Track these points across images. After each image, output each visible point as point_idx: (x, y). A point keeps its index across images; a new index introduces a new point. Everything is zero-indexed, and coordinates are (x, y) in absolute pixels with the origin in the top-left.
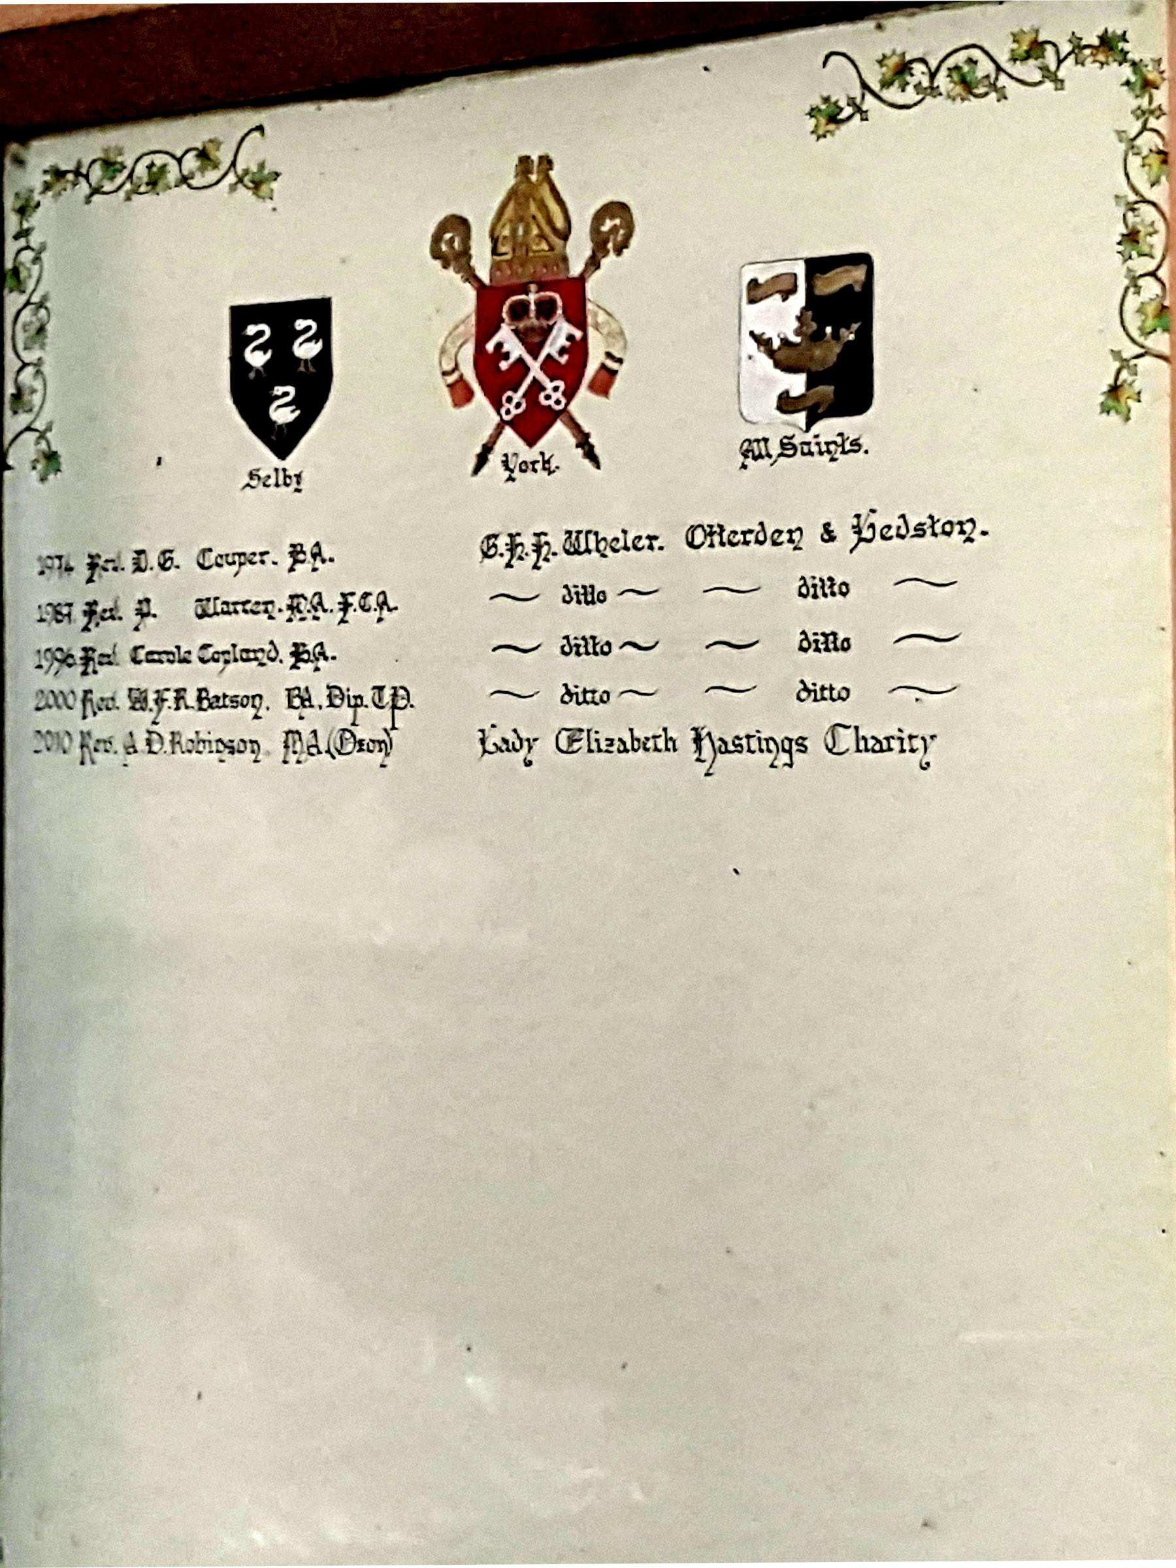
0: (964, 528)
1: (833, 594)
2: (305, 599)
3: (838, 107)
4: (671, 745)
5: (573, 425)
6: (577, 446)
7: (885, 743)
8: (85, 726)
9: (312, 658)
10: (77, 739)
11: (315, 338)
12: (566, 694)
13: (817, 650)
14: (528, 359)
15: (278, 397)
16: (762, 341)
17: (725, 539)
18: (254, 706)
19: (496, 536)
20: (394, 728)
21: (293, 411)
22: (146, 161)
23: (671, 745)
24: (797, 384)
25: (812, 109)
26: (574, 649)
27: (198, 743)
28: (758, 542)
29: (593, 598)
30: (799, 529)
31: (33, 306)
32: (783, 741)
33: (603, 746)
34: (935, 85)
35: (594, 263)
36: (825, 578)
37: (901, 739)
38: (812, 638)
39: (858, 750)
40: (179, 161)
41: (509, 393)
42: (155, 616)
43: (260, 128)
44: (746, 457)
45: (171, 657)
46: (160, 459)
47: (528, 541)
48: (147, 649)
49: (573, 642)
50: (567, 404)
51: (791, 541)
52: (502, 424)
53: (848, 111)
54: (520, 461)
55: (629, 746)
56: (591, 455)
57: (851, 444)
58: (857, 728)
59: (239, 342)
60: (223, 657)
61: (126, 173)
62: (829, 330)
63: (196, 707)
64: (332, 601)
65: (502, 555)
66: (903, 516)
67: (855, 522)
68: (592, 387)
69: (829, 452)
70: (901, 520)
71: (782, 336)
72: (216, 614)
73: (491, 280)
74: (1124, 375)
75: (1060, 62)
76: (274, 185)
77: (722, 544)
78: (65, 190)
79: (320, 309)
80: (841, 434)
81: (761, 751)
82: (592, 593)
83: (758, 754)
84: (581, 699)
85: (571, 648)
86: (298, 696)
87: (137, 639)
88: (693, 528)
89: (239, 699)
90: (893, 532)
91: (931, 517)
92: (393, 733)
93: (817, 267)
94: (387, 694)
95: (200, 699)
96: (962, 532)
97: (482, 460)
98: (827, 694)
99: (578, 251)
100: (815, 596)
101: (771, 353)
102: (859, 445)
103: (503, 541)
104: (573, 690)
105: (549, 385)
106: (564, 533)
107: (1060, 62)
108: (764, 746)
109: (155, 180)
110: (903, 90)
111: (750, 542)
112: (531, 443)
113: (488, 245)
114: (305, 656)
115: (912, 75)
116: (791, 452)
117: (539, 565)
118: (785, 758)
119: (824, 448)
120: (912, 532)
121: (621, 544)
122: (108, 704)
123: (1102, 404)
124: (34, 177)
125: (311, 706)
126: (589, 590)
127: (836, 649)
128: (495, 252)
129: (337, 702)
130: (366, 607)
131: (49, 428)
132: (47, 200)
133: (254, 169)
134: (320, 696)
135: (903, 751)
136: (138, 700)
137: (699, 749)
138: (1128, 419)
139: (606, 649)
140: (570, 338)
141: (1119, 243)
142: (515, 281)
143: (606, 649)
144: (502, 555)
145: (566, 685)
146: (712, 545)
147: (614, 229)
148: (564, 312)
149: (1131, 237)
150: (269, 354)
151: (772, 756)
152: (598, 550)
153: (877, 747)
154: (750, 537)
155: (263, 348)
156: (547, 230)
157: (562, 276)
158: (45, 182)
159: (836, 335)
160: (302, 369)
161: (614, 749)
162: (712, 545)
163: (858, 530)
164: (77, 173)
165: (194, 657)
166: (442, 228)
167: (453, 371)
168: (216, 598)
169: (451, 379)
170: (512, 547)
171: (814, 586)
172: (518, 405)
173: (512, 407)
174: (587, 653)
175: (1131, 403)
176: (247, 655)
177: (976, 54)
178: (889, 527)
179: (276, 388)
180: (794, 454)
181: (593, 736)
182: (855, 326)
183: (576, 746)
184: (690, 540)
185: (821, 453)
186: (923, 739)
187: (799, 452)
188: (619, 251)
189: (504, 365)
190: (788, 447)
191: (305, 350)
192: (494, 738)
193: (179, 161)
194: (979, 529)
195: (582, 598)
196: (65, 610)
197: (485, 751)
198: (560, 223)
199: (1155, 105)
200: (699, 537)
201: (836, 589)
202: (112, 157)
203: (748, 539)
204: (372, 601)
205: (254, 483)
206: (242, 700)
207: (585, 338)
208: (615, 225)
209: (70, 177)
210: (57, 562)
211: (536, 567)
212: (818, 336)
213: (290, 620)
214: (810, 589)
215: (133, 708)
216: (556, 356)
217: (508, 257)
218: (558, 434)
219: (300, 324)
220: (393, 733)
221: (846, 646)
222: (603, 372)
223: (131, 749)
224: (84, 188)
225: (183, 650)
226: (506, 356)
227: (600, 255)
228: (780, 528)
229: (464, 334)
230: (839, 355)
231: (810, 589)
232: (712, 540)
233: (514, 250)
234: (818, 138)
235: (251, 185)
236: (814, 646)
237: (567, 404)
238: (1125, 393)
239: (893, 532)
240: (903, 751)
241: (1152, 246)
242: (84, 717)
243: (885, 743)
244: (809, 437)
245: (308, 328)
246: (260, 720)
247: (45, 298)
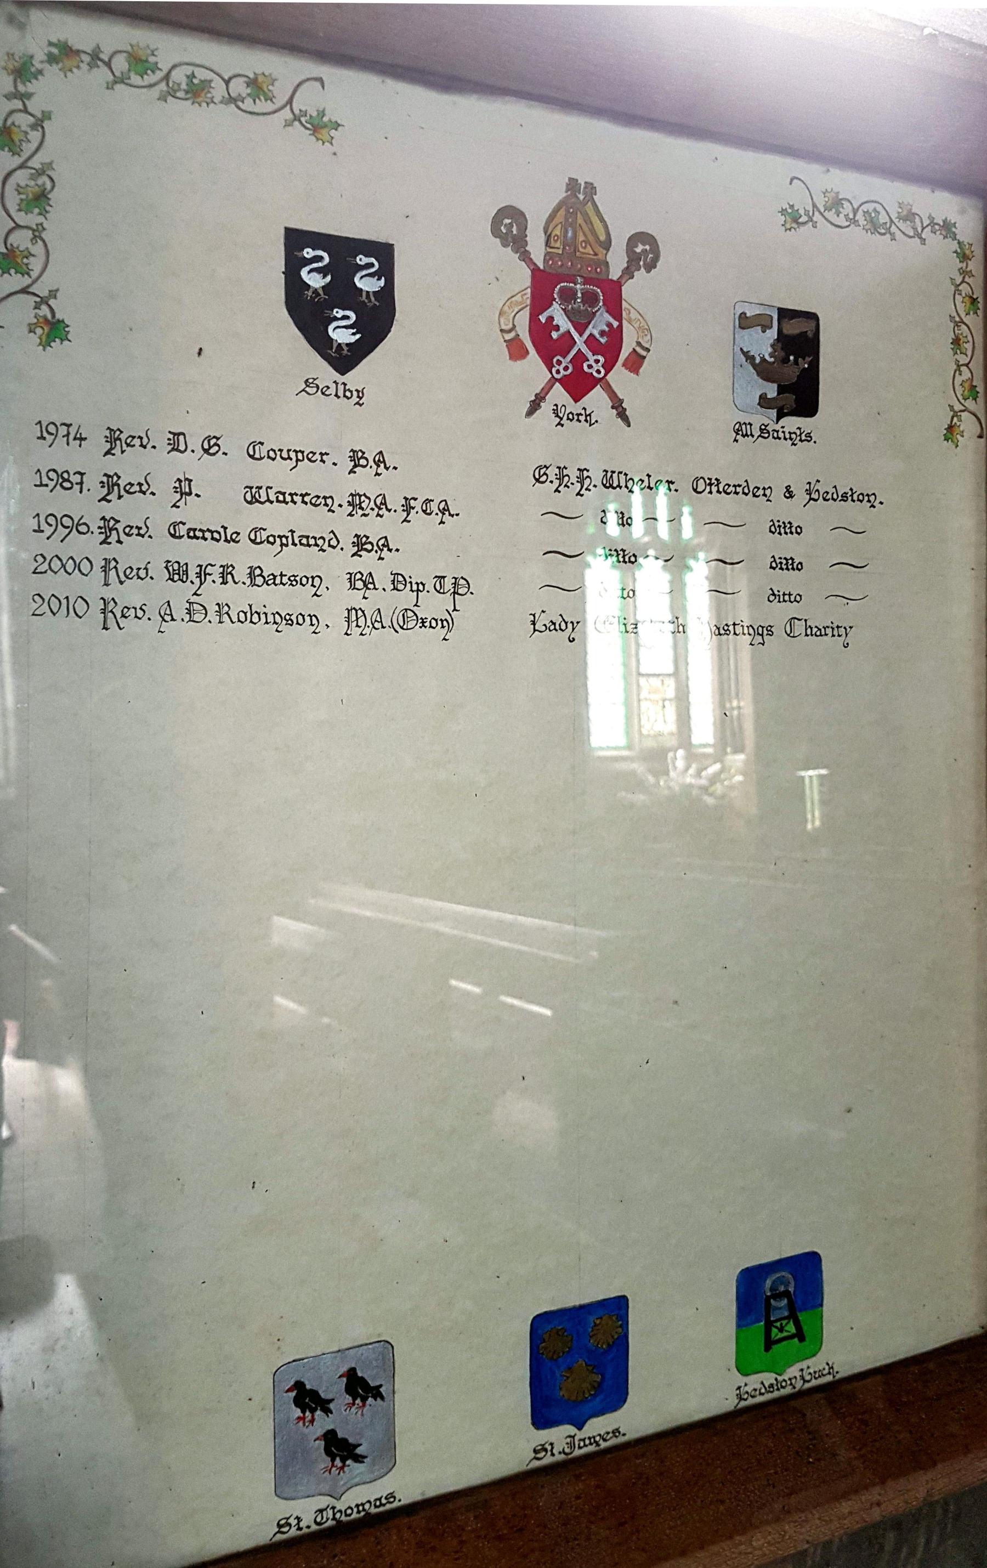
0: (868, 499)
3: (798, 213)
7: (823, 630)
8: (108, 593)
13: (781, 569)
14: (576, 335)
15: (336, 319)
18: (313, 585)
20: (455, 610)
21: (354, 334)
27: (251, 615)
28: (744, 493)
34: (856, 219)
36: (786, 522)
38: (778, 561)
39: (807, 635)
44: (738, 434)
46: (201, 349)
47: (573, 474)
50: (606, 375)
51: (765, 495)
57: (806, 436)
58: (806, 620)
60: (283, 541)
61: (159, 75)
62: (792, 358)
64: (395, 502)
65: (551, 482)
66: (835, 487)
67: (808, 487)
69: (791, 439)
70: (834, 489)
74: (955, 419)
75: (923, 229)
80: (799, 428)
87: (176, 515)
88: (697, 479)
90: (829, 496)
91: (851, 489)
92: (454, 614)
93: (784, 314)
95: (251, 575)
98: (787, 598)
100: (780, 533)
101: (755, 366)
103: (552, 472)
106: (602, 471)
107: (923, 229)
108: (746, 631)
110: (838, 216)
111: (739, 493)
112: (576, 401)
113: (542, 238)
114: (369, 547)
115: (843, 208)
117: (581, 493)
118: (759, 639)
119: (787, 436)
120: (840, 498)
122: (141, 573)
123: (944, 435)
128: (547, 244)
129: (401, 587)
130: (428, 511)
135: (833, 636)
136: (177, 573)
138: (957, 446)
139: (633, 559)
140: (609, 325)
141: (952, 343)
143: (633, 559)
144: (551, 482)
146: (711, 492)
147: (644, 251)
149: (956, 342)
150: (329, 278)
152: (626, 487)
153: (818, 633)
154: (739, 489)
155: (323, 271)
156: (591, 238)
159: (796, 362)
163: (809, 492)
165: (243, 537)
167: (510, 331)
169: (509, 336)
170: (561, 478)
171: (779, 526)
172: (566, 368)
175: (958, 436)
176: (306, 541)
177: (879, 208)
182: (808, 359)
184: (695, 487)
186: (845, 628)
187: (771, 436)
192: (541, 622)
197: (535, 630)
198: (603, 237)
199: (968, 269)
200: (701, 487)
201: (794, 530)
203: (738, 491)
204: (434, 507)
207: (620, 326)
210: (63, 430)
212: (786, 360)
218: (596, 399)
219: (362, 260)
220: (454, 614)
221: (800, 567)
222: (634, 356)
226: (557, 328)
227: (633, 268)
228: (758, 486)
229: (521, 303)
234: (786, 230)
236: (779, 566)
237: (606, 375)
238: (956, 431)
239: (829, 496)
240: (833, 636)
241: (966, 349)
243: (823, 630)
244: (778, 427)
245: (371, 265)
246: (103, 454)
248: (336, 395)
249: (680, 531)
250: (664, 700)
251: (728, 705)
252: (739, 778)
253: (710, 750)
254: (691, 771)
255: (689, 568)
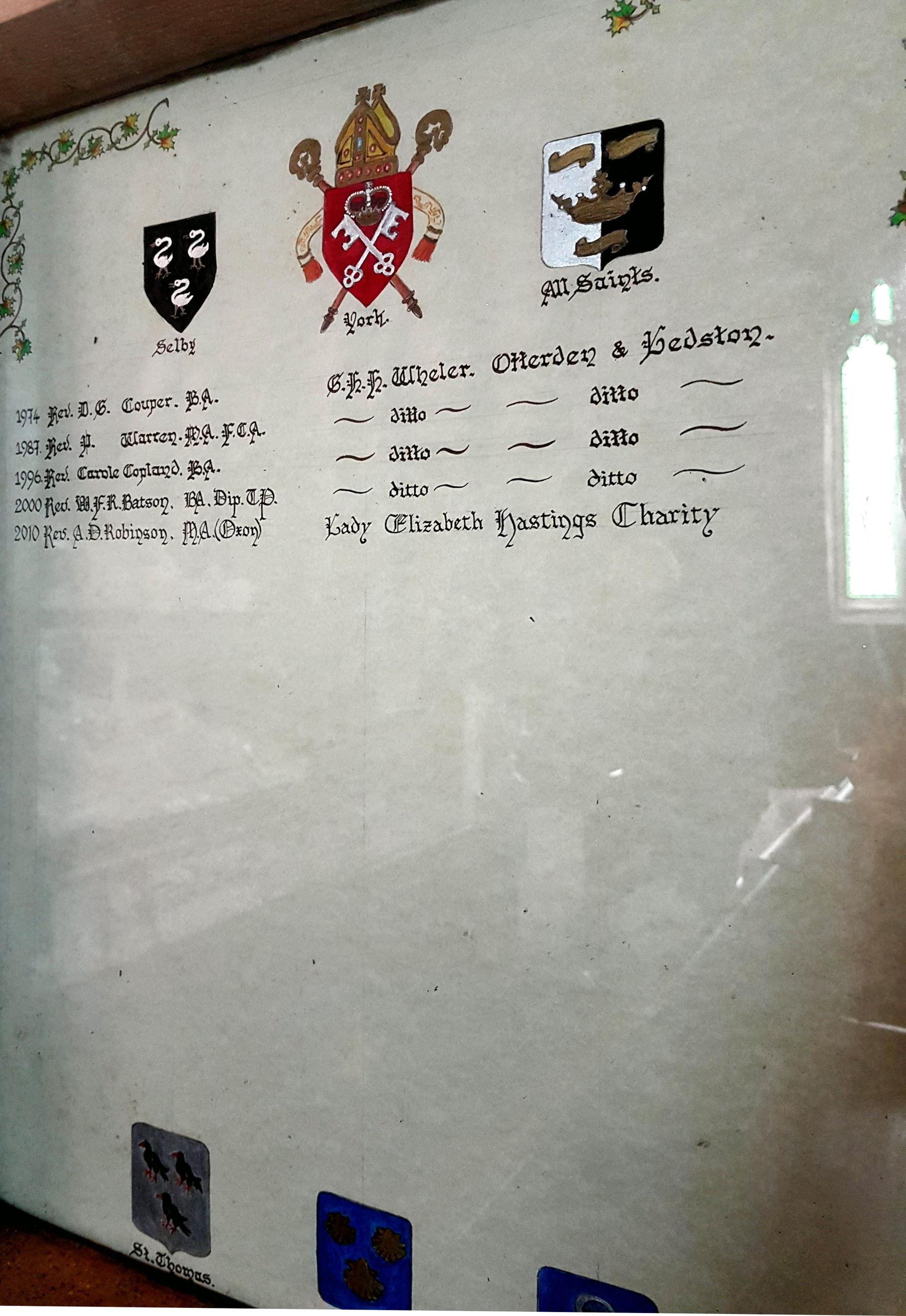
1: (623, 399)
2: (198, 430)
4: (479, 524)
5: (401, 286)
6: (404, 302)
8: (47, 522)
9: (203, 471)
10: (43, 531)
11: (204, 242)
12: (393, 489)
14: (365, 239)
15: (177, 288)
16: (563, 203)
17: (526, 364)
18: (162, 506)
19: (339, 376)
20: (262, 518)
21: (188, 297)
22: (88, 136)
23: (479, 524)
24: (593, 232)
25: (608, 12)
26: (400, 456)
28: (555, 362)
29: (415, 417)
30: (593, 349)
31: (15, 245)
32: (574, 519)
33: (422, 527)
35: (418, 159)
36: (616, 387)
37: (685, 513)
40: (110, 133)
41: (350, 267)
42: (93, 446)
43: (166, 101)
45: (105, 474)
46: (96, 339)
47: (364, 377)
48: (88, 469)
49: (399, 451)
50: (396, 270)
52: (345, 290)
53: (640, 9)
54: (358, 318)
55: (443, 527)
56: (415, 308)
58: (642, 505)
59: (150, 252)
60: (142, 472)
61: (74, 146)
63: (122, 508)
64: (217, 430)
67: (646, 338)
68: (416, 255)
69: (621, 284)
71: (580, 195)
72: (136, 443)
73: (336, 185)
76: (175, 139)
77: (524, 367)
78: (35, 164)
79: (207, 222)
81: (555, 526)
82: (415, 414)
83: (552, 529)
84: (405, 493)
85: (398, 455)
86: (193, 498)
87: (82, 463)
89: (152, 501)
91: (718, 328)
93: (610, 136)
94: (258, 494)
95: (124, 502)
96: (749, 338)
97: (329, 319)
98: (615, 479)
99: (405, 152)
100: (606, 402)
101: (570, 210)
102: (651, 275)
104: (398, 486)
105: (381, 257)
109: (94, 149)
112: (366, 304)
113: (334, 157)
114: (198, 470)
116: (587, 287)
118: (577, 531)
119: (617, 281)
121: (439, 373)
122: (62, 507)
124: (16, 159)
125: (203, 505)
126: (413, 411)
127: (624, 443)
128: (339, 162)
129: (222, 501)
130: (242, 434)
131: (23, 324)
132: (23, 174)
133: (162, 129)
134: (208, 497)
136: (83, 504)
137: (502, 526)
139: (425, 454)
140: (399, 219)
142: (355, 181)
143: (425, 454)
144: (344, 389)
145: (393, 483)
146: (515, 369)
147: (436, 131)
148: (393, 200)
151: (565, 530)
152: (419, 380)
157: (391, 173)
158: (23, 161)
159: (629, 189)
160: (195, 265)
161: (431, 528)
162: (515, 369)
163: (648, 345)
164: (43, 152)
165: (121, 474)
166: (299, 149)
168: (136, 432)
169: (304, 262)
172: (356, 276)
173: (352, 277)
174: (410, 458)
176: (158, 471)
178: (678, 340)
179: (176, 282)
180: (590, 288)
181: (414, 519)
183: (401, 527)
184: (496, 367)
185: (614, 285)
186: (706, 511)
188: (439, 149)
189: (346, 246)
190: (583, 284)
191: (196, 252)
192: (337, 523)
193: (110, 133)
194: (764, 335)
195: (407, 418)
196: (34, 446)
197: (330, 533)
198: (391, 133)
200: (503, 365)
201: (626, 395)
202: (65, 137)
204: (246, 429)
205: (160, 350)
206: (154, 502)
207: (411, 217)
208: (437, 128)
209: (39, 155)
211: (370, 397)
213: (187, 445)
214: (600, 397)
215: (80, 509)
216: (387, 234)
217: (350, 164)
219: (194, 233)
221: (634, 440)
223: (78, 537)
224: (47, 161)
225: (112, 470)
230: (631, 205)
231: (600, 397)
232: (515, 365)
233: (354, 159)
235: (159, 141)
237: (396, 270)
239: (681, 343)
242: (47, 516)
247: (22, 238)
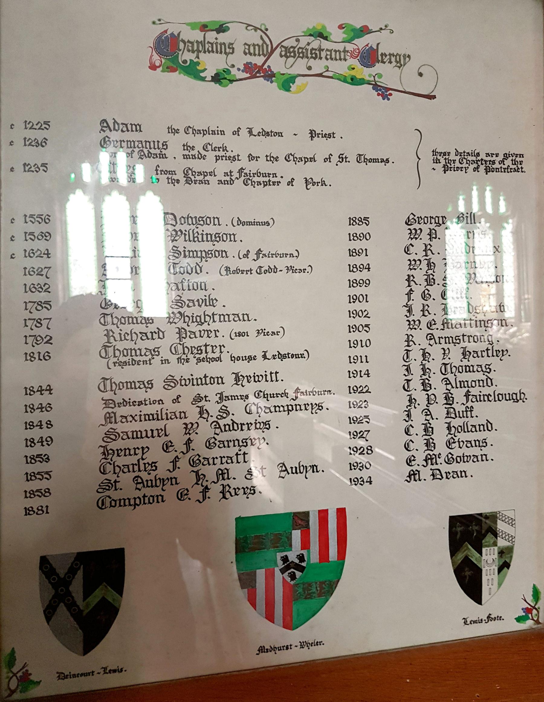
248: (229, 315)
249: (498, 209)
250: (489, 295)
251: (523, 297)
252: (527, 335)
253: (513, 320)
254: (501, 331)
255: (504, 228)
